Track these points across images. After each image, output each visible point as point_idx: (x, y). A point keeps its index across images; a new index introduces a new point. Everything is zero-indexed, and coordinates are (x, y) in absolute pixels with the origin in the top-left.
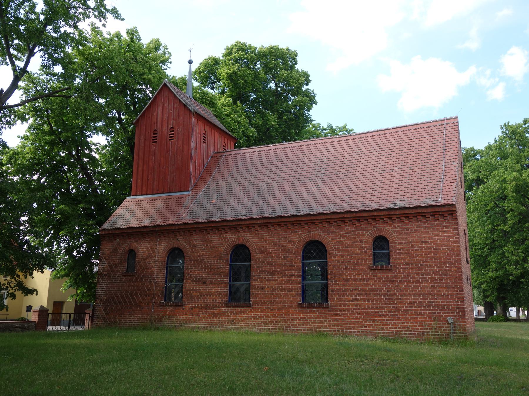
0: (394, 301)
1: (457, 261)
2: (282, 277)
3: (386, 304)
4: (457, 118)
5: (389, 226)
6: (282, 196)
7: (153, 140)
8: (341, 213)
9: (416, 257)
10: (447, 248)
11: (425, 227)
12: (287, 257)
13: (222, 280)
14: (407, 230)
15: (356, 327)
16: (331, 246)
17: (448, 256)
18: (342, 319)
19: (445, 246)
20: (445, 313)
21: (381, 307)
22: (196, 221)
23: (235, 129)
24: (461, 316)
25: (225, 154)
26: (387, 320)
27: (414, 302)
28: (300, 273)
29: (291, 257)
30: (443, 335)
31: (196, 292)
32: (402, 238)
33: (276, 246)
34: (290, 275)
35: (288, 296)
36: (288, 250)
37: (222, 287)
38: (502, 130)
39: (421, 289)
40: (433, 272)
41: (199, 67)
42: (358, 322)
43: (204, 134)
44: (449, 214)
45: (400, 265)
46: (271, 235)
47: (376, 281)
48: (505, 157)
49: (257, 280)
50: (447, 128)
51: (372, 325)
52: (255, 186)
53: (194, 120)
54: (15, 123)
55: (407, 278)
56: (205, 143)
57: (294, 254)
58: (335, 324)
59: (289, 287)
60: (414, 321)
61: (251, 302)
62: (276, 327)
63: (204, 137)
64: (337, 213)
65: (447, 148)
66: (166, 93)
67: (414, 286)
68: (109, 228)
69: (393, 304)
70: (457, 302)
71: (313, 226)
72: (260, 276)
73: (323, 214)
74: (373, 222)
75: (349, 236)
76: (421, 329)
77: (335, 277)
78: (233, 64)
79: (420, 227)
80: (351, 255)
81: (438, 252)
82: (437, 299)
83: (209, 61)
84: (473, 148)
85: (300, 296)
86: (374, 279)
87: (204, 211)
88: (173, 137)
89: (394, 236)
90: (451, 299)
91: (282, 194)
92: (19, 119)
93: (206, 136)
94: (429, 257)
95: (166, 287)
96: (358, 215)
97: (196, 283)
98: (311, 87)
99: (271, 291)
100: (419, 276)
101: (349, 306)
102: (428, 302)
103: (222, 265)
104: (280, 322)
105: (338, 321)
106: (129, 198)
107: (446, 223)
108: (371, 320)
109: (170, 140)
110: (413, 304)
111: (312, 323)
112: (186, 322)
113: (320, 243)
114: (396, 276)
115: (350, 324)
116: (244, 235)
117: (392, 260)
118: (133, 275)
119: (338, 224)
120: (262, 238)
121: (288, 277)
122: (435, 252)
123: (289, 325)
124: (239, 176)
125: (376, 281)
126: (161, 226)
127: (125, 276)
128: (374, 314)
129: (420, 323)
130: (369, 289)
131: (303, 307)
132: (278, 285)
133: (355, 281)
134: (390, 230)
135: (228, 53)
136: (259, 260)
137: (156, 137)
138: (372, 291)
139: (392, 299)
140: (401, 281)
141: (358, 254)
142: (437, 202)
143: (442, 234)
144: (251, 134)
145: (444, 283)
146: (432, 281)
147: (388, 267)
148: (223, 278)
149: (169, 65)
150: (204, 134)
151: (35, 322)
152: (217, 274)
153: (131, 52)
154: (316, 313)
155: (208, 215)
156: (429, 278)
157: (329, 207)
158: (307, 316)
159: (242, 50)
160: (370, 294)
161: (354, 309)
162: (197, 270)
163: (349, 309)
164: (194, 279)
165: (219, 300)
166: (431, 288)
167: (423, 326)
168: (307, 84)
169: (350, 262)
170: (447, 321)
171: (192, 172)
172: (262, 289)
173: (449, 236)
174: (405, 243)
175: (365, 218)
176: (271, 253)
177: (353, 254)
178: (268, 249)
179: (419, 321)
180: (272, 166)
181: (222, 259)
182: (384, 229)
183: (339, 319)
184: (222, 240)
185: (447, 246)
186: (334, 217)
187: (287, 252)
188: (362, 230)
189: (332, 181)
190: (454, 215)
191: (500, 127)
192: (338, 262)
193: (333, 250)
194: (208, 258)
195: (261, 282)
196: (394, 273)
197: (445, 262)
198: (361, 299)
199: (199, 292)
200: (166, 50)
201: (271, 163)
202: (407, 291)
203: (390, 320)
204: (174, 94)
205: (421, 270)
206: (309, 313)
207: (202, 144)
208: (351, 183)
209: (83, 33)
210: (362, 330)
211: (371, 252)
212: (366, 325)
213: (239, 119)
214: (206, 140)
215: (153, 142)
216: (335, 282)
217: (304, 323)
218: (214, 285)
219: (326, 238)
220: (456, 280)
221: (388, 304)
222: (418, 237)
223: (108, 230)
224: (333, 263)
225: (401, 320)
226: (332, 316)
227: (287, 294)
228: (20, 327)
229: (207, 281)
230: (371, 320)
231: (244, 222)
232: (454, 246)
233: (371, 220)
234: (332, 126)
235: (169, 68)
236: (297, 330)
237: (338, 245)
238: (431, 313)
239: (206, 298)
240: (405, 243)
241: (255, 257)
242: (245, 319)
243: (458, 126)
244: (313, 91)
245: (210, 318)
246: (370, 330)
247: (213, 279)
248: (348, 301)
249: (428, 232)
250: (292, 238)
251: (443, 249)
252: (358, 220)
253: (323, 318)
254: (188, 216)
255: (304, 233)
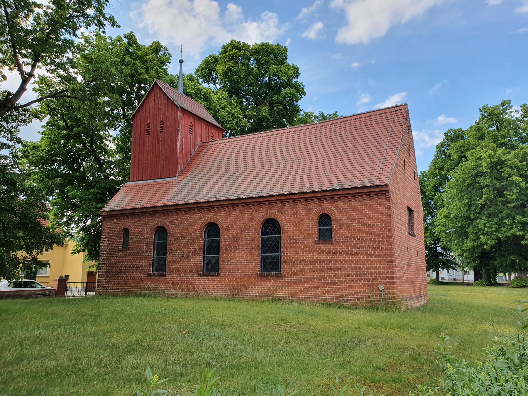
0: (335, 271)
1: (388, 236)
2: (245, 250)
3: (328, 273)
4: (406, 105)
5: (332, 205)
6: (334, 178)
7: (147, 132)
8: (291, 194)
9: (354, 232)
10: (380, 224)
11: (362, 205)
12: (249, 233)
13: (197, 254)
14: (346, 209)
15: (304, 293)
16: (284, 222)
17: (381, 231)
18: (292, 286)
19: (378, 222)
20: (377, 282)
21: (324, 276)
22: (176, 203)
23: (229, 121)
24: (390, 284)
25: (210, 143)
26: (329, 287)
27: (352, 272)
28: (259, 246)
29: (252, 232)
30: (375, 301)
31: (176, 264)
32: (342, 215)
33: (240, 224)
34: (251, 248)
35: (249, 266)
36: (250, 227)
37: (197, 260)
38: (481, 113)
39: (358, 260)
40: (368, 246)
41: (201, 64)
42: (300, 289)
43: (190, 126)
44: (382, 194)
45: (340, 240)
46: (237, 214)
47: (320, 253)
48: (482, 137)
49: (225, 253)
50: (396, 115)
51: (316, 291)
52: (229, 171)
53: (180, 114)
54: (31, 121)
55: (346, 251)
56: (192, 134)
57: (255, 230)
58: (286, 290)
59: (250, 258)
60: (351, 288)
61: (220, 272)
62: (239, 293)
63: (190, 128)
64: (288, 194)
65: (392, 133)
66: (157, 90)
67: (351, 257)
68: (108, 210)
69: (334, 273)
70: (387, 272)
71: (270, 206)
72: (227, 249)
73: (277, 195)
74: (319, 202)
75: (298, 214)
76: (357, 295)
77: (286, 250)
78: (228, 61)
79: (357, 206)
80: (299, 231)
81: (372, 227)
82: (370, 269)
83: (210, 59)
84: (461, 129)
85: (259, 267)
86: (318, 251)
87: (185, 194)
88: (163, 129)
89: (335, 214)
90: (382, 269)
91: (333, 176)
92: (33, 117)
93: (193, 128)
94: (365, 232)
95: (153, 260)
96: (306, 196)
97: (176, 256)
98: (300, 79)
99: (236, 263)
100: (356, 248)
101: (297, 275)
102: (363, 272)
103: (198, 241)
104: (242, 289)
105: (289, 288)
106: (128, 184)
107: (380, 202)
108: (315, 287)
109: (160, 132)
110: (351, 274)
111: (268, 290)
112: (168, 290)
113: (276, 221)
114: (336, 248)
115: (299, 291)
116: (215, 214)
117: (333, 235)
118: (127, 250)
119: (290, 204)
120: (230, 217)
121: (249, 250)
122: (370, 227)
123: (249, 291)
124: (219, 163)
125: (320, 253)
126: (149, 207)
127: (121, 251)
128: (318, 282)
129: (356, 291)
130: (314, 260)
131: (261, 276)
132: (242, 257)
133: (303, 253)
134: (333, 209)
135: (224, 51)
136: (227, 236)
137: (149, 129)
138: (317, 262)
139: (333, 269)
140: (341, 253)
141: (305, 230)
142: (373, 183)
143: (376, 211)
144: (244, 125)
145: (377, 255)
146: (367, 253)
147: (330, 241)
148: (198, 252)
149: (169, 65)
150: (190, 126)
151: (55, 289)
152: (193, 249)
153: (129, 54)
154: (271, 281)
155: (187, 197)
156: (364, 250)
157: (282, 190)
158: (264, 283)
159: (236, 48)
160: (315, 264)
161: (302, 278)
162: (177, 246)
163: (298, 278)
164: (174, 253)
165: (194, 271)
166: (366, 260)
167: (358, 293)
168: (297, 77)
169: (299, 236)
170: (379, 289)
171: (178, 161)
172: (229, 261)
173: (382, 213)
174: (345, 220)
175: (312, 198)
176: (236, 229)
177: (301, 230)
178: (233, 226)
179: (356, 288)
180: (246, 153)
181: (197, 235)
182: (327, 208)
183: (289, 286)
184: (197, 219)
185: (381, 222)
186: (285, 198)
187: (249, 229)
188: (309, 209)
189: (360, 161)
190: (386, 194)
191: (479, 110)
192: (290, 237)
193: (286, 227)
194: (187, 234)
195: (228, 255)
196: (335, 246)
197: (378, 236)
198: (308, 269)
199: (178, 264)
200: (166, 52)
201: (246, 151)
202: (346, 262)
203: (332, 287)
204: (163, 92)
205: (358, 244)
206: (265, 281)
207: (189, 135)
208: (361, 163)
209: (89, 38)
210: (308, 296)
211: (316, 228)
212: (312, 291)
213: (233, 111)
214: (193, 131)
215: (147, 135)
216: (287, 254)
217: (262, 290)
218: (191, 258)
219: (280, 216)
220: (388, 252)
221: (330, 273)
222: (356, 214)
223: (107, 211)
224: (285, 237)
225: (341, 288)
226: (284, 284)
227: (248, 264)
228: (42, 294)
229: (185, 254)
230: (315, 287)
231: (214, 204)
232: (386, 222)
233: (316, 200)
234: (323, 114)
235: (169, 67)
236: (256, 296)
237: (289, 222)
238: (365, 281)
239: (184, 269)
240: (345, 220)
241: (224, 234)
242: (214, 287)
243: (408, 113)
244: (301, 83)
245: (187, 286)
246: (315, 296)
247: (190, 252)
248: (297, 271)
249: (364, 209)
250: (253, 217)
251: (377, 225)
252: (306, 200)
253: (277, 286)
254: (171, 199)
255: (262, 212)
